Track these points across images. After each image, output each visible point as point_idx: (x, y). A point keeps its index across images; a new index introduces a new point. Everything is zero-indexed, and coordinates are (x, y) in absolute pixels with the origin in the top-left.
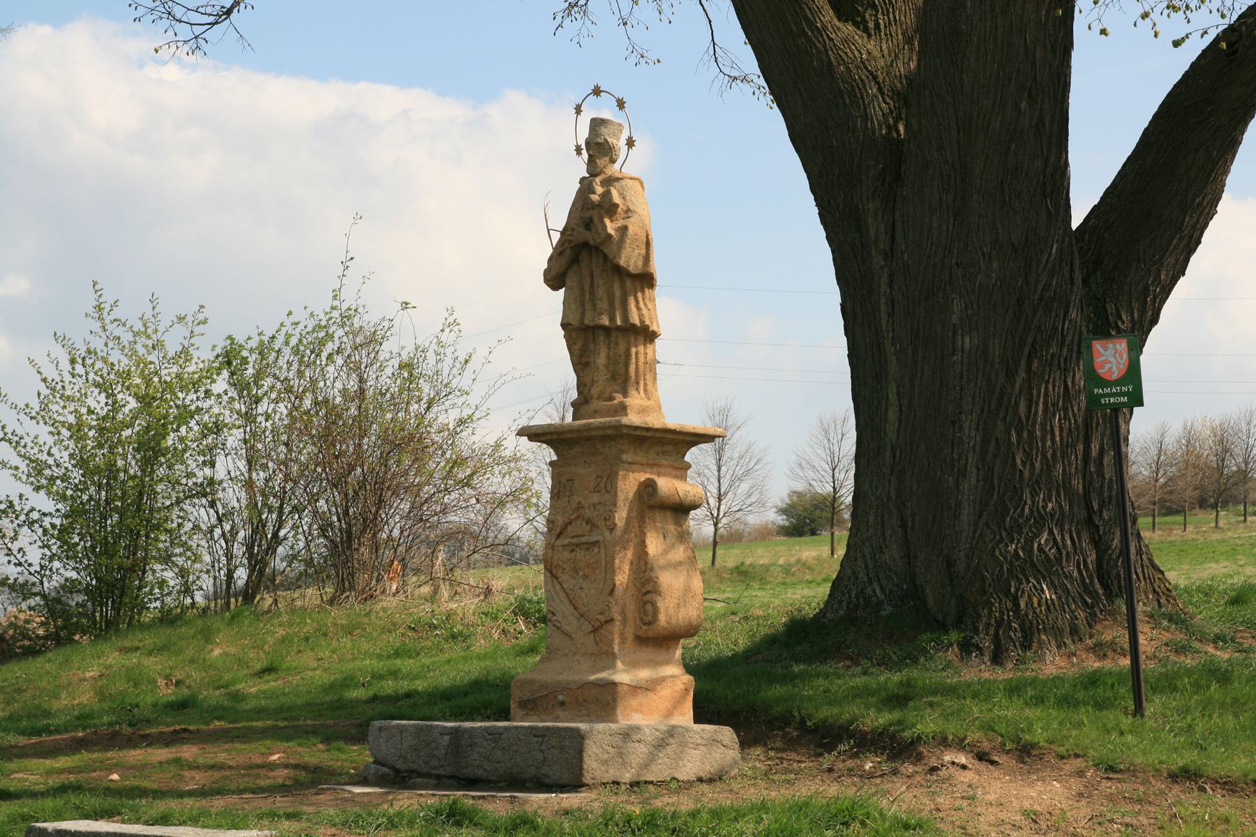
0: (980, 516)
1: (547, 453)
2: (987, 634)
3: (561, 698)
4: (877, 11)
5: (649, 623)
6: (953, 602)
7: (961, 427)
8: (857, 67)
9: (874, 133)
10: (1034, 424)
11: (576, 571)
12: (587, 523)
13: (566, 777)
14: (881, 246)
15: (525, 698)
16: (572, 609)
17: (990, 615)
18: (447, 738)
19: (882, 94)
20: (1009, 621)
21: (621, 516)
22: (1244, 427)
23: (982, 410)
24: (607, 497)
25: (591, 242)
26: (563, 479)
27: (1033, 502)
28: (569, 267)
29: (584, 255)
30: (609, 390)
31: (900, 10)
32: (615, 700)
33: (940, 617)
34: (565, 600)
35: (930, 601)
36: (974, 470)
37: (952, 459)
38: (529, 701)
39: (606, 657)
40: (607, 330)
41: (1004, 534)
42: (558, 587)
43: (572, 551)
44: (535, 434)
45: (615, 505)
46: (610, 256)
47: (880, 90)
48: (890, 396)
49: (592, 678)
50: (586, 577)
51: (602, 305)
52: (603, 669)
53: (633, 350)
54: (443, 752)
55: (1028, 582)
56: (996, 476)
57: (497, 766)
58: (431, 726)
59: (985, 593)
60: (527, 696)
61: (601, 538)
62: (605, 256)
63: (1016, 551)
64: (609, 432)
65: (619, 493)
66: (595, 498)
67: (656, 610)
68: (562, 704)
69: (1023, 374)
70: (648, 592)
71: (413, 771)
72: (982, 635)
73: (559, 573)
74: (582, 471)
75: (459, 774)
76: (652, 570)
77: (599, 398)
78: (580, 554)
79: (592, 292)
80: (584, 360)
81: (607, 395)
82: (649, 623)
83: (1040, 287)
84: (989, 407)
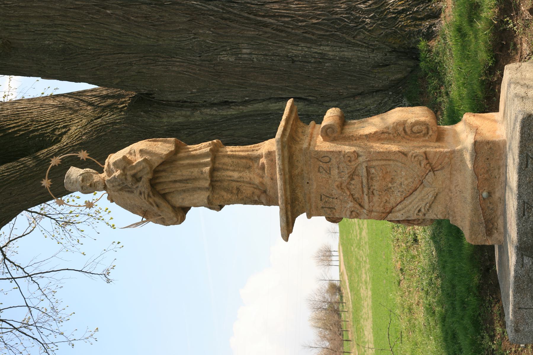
0: (349, 43)
1: (301, 220)
2: (421, 25)
3: (485, 194)
4: (57, 128)
5: (428, 129)
6: (401, 62)
7: (296, 56)
8: (85, 129)
9: (123, 118)
10: (296, 14)
11: (388, 190)
12: (352, 179)
14: (188, 113)
15: (484, 230)
16: (416, 193)
17: (409, 26)
18: (526, 260)
19: (101, 116)
20: (414, 12)
21: (347, 149)
22: (311, 302)
23: (287, 42)
24: (334, 161)
25: (150, 176)
26: (321, 204)
27: (341, 13)
28: (168, 202)
29: (159, 188)
30: (257, 171)
31: (58, 117)
32: (488, 143)
33: (409, 69)
34: (410, 200)
35: (399, 76)
36: (322, 48)
37: (314, 62)
38: (486, 227)
39: (454, 157)
40: (213, 170)
41: (360, 26)
42: (399, 207)
43: (373, 194)
44: (287, 228)
45: (340, 152)
46: (160, 161)
47: (99, 118)
48: (277, 108)
49: (470, 165)
50: (392, 181)
51: (195, 172)
52: (463, 161)
53: (229, 153)
55: (389, 9)
56: (326, 33)
58: (516, 277)
59: (395, 32)
61: (365, 165)
62: (162, 164)
63: (370, 18)
64: (286, 154)
65: (332, 150)
66: (335, 172)
67: (417, 123)
68: (490, 194)
69: (266, 19)
70: (404, 130)
72: (422, 28)
73: (389, 206)
74: (315, 187)
76: (388, 128)
77: (262, 177)
78: (376, 185)
79: (186, 181)
80: (235, 191)
81: (260, 172)
82: (428, 129)
83: (216, 9)
84: (285, 37)
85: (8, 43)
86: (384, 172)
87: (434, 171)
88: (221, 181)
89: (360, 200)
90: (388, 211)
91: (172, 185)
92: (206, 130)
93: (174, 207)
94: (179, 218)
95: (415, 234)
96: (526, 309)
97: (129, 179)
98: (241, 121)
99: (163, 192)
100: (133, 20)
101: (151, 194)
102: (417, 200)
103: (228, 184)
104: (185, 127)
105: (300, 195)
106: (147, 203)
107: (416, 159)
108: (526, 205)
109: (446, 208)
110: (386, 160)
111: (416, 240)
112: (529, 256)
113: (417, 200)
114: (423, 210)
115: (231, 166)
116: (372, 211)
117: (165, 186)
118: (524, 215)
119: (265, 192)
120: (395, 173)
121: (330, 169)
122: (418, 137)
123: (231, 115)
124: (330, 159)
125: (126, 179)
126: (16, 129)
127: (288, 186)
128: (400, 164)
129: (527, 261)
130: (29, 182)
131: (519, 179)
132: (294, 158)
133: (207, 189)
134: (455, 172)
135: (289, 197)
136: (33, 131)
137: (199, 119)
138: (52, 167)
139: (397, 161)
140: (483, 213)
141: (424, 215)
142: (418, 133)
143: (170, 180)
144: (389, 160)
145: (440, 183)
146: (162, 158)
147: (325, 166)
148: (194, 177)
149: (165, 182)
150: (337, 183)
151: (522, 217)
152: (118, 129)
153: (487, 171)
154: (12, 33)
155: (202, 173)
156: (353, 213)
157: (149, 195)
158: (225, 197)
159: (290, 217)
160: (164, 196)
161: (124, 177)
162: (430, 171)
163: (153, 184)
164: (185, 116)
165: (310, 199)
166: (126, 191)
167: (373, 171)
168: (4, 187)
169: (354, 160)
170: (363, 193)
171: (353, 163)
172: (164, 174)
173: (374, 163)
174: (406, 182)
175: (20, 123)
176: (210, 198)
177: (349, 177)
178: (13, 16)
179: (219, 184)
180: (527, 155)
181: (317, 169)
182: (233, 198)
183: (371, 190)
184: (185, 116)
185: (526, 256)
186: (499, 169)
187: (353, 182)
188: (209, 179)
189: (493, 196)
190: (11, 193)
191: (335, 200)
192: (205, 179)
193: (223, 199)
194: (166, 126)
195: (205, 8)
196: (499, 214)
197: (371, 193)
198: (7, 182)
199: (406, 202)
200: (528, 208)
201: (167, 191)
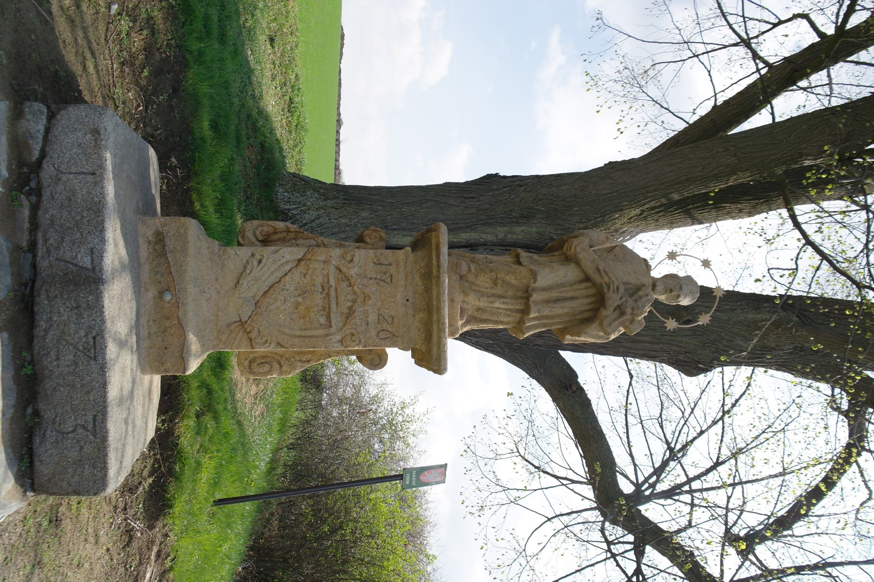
3: (168, 297)
11: (303, 293)
12: (350, 308)
13: (44, 469)
14: (509, 236)
15: (168, 242)
18: (86, 262)
24: (373, 333)
25: (604, 313)
28: (583, 271)
34: (273, 279)
38: (164, 246)
43: (323, 287)
49: (192, 338)
50: (297, 305)
54: (68, 256)
57: (53, 355)
60: (170, 244)
61: (333, 330)
66: (372, 318)
70: (281, 367)
71: (39, 195)
73: (302, 268)
75: (38, 285)
78: (319, 299)
79: (557, 300)
80: (500, 282)
82: (250, 367)
86: (307, 319)
87: (241, 321)
89: (340, 276)
90: (303, 263)
91: (577, 294)
93: (578, 263)
94: (573, 250)
95: (273, 47)
96: (83, 173)
97: (629, 310)
98: (457, 223)
99: (588, 284)
101: (606, 290)
102: (263, 278)
104: (514, 220)
105: (418, 281)
107: (265, 339)
108: (92, 355)
109: (223, 266)
110: (306, 337)
111: (272, 40)
112: (82, 268)
113: (263, 278)
114: (255, 263)
116: (324, 262)
117: (585, 292)
118: (94, 338)
119: (462, 277)
120: (292, 316)
121: (379, 323)
122: (263, 357)
123: (465, 232)
124: (378, 335)
125: (633, 309)
127: (435, 303)
128: (286, 331)
129: (85, 259)
131: (105, 396)
132: (423, 335)
134: (212, 318)
135: (434, 287)
136: (660, 212)
137: (499, 229)
139: (290, 335)
140: (169, 267)
141: (253, 255)
142: (262, 363)
143: (578, 302)
144: (301, 336)
145: (231, 304)
146: (586, 333)
147: (385, 326)
148: (549, 305)
150: (370, 302)
151: (97, 335)
152: (583, 223)
153: (166, 331)
155: (539, 311)
156: (350, 259)
157: (609, 288)
158: (513, 278)
159: (434, 257)
160: (587, 279)
162: (246, 322)
163: (600, 301)
164: (513, 233)
165: (406, 277)
167: (323, 320)
169: (347, 335)
170: (336, 289)
171: (348, 332)
173: (321, 332)
174: (278, 304)
176: (532, 281)
177: (354, 312)
179: (519, 294)
180: (95, 436)
181: (396, 320)
182: (503, 275)
183: (325, 292)
184: (513, 233)
185: (87, 269)
186: (149, 334)
187: (349, 304)
188: (531, 303)
189: (156, 293)
191: (374, 276)
196: (146, 266)
197: (325, 288)
199: (278, 274)
200: (89, 351)
201: (583, 285)
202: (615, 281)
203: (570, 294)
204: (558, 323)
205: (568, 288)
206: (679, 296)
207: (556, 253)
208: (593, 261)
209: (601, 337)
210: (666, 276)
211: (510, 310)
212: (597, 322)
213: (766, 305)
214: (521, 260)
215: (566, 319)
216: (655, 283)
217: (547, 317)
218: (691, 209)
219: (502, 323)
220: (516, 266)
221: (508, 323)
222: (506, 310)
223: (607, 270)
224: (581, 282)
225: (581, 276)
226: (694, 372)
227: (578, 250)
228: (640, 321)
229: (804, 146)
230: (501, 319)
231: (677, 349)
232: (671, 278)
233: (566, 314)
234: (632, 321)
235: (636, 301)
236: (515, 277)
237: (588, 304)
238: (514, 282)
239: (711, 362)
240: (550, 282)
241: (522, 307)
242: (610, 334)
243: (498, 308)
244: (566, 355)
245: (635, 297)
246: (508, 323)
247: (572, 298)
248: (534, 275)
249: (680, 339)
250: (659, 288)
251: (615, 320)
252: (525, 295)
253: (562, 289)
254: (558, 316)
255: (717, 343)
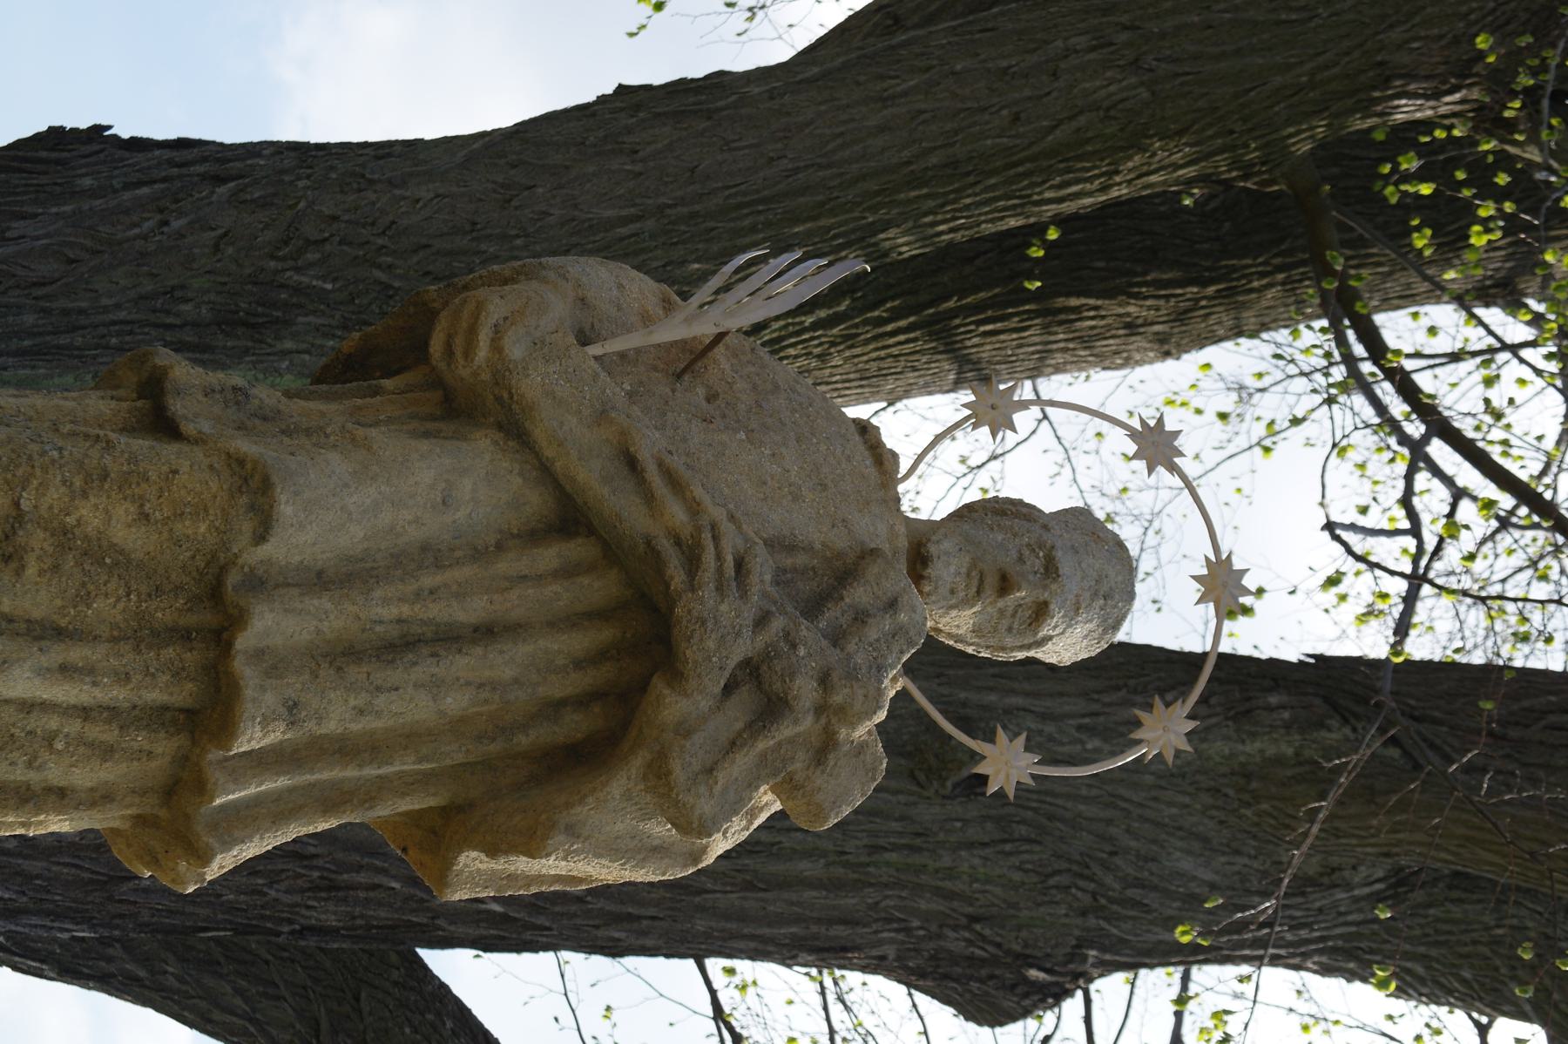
25: (672, 706)
28: (546, 473)
79: (400, 646)
85: (922, 777)
88: (141, 635)
91: (514, 604)
92: (81, 311)
93: (514, 429)
94: (482, 352)
97: (805, 690)
99: (579, 549)
100: (394, 877)
101: (677, 575)
103: (85, 598)
106: (698, 492)
115: (50, 739)
117: (562, 596)
125: (824, 680)
126: (889, 328)
130: (934, 160)
133: (258, 583)
138: (1184, 696)
143: (523, 650)
146: (572, 831)
148: (355, 673)
149: (556, 624)
154: (902, 818)
155: (292, 708)
157: (693, 562)
158: (123, 511)
160: (570, 517)
161: (837, 699)
163: (643, 635)
166: (809, 549)
168: (1035, 149)
172: (559, 688)
175: (871, 347)
176: (247, 527)
178: (886, 885)
179: (164, 613)
182: (55, 495)
188: (240, 665)
190: (1016, 118)
192: (274, 664)
193: (141, 501)
194: (285, 353)
195: (35, 920)
198: (1020, 169)
201: (549, 556)
202: (726, 527)
203: (473, 610)
204: (409, 784)
205: (465, 572)
206: (1040, 612)
207: (387, 383)
208: (602, 415)
209: (658, 851)
210: (966, 513)
211: (111, 712)
212: (638, 762)
213: (1273, 700)
214: (177, 406)
215: (455, 753)
216: (920, 546)
217: (343, 749)
218: (953, 313)
219: (60, 797)
220: (141, 444)
221: (101, 797)
222: (85, 713)
223: (676, 462)
224: (534, 536)
225: (537, 502)
226: (1009, 1004)
227: (515, 350)
228: (861, 748)
229: (1396, 35)
230: (55, 773)
231: (937, 905)
232: (996, 516)
233: (457, 726)
234: (824, 748)
235: (837, 638)
236: (137, 513)
237: (579, 664)
238: (126, 533)
239: (1076, 955)
240: (352, 537)
241: (182, 695)
242: (706, 829)
243: (28, 706)
244: (460, 970)
245: (832, 614)
246: (101, 797)
247: (487, 632)
248: (255, 490)
249: (947, 861)
250: (948, 568)
251: (733, 745)
252: (205, 617)
253: (428, 581)
254: (411, 738)
255: (1097, 870)
